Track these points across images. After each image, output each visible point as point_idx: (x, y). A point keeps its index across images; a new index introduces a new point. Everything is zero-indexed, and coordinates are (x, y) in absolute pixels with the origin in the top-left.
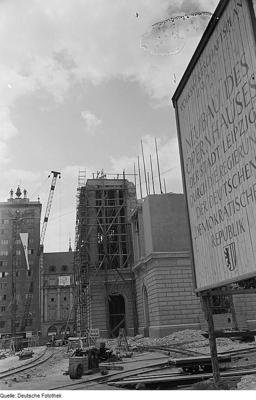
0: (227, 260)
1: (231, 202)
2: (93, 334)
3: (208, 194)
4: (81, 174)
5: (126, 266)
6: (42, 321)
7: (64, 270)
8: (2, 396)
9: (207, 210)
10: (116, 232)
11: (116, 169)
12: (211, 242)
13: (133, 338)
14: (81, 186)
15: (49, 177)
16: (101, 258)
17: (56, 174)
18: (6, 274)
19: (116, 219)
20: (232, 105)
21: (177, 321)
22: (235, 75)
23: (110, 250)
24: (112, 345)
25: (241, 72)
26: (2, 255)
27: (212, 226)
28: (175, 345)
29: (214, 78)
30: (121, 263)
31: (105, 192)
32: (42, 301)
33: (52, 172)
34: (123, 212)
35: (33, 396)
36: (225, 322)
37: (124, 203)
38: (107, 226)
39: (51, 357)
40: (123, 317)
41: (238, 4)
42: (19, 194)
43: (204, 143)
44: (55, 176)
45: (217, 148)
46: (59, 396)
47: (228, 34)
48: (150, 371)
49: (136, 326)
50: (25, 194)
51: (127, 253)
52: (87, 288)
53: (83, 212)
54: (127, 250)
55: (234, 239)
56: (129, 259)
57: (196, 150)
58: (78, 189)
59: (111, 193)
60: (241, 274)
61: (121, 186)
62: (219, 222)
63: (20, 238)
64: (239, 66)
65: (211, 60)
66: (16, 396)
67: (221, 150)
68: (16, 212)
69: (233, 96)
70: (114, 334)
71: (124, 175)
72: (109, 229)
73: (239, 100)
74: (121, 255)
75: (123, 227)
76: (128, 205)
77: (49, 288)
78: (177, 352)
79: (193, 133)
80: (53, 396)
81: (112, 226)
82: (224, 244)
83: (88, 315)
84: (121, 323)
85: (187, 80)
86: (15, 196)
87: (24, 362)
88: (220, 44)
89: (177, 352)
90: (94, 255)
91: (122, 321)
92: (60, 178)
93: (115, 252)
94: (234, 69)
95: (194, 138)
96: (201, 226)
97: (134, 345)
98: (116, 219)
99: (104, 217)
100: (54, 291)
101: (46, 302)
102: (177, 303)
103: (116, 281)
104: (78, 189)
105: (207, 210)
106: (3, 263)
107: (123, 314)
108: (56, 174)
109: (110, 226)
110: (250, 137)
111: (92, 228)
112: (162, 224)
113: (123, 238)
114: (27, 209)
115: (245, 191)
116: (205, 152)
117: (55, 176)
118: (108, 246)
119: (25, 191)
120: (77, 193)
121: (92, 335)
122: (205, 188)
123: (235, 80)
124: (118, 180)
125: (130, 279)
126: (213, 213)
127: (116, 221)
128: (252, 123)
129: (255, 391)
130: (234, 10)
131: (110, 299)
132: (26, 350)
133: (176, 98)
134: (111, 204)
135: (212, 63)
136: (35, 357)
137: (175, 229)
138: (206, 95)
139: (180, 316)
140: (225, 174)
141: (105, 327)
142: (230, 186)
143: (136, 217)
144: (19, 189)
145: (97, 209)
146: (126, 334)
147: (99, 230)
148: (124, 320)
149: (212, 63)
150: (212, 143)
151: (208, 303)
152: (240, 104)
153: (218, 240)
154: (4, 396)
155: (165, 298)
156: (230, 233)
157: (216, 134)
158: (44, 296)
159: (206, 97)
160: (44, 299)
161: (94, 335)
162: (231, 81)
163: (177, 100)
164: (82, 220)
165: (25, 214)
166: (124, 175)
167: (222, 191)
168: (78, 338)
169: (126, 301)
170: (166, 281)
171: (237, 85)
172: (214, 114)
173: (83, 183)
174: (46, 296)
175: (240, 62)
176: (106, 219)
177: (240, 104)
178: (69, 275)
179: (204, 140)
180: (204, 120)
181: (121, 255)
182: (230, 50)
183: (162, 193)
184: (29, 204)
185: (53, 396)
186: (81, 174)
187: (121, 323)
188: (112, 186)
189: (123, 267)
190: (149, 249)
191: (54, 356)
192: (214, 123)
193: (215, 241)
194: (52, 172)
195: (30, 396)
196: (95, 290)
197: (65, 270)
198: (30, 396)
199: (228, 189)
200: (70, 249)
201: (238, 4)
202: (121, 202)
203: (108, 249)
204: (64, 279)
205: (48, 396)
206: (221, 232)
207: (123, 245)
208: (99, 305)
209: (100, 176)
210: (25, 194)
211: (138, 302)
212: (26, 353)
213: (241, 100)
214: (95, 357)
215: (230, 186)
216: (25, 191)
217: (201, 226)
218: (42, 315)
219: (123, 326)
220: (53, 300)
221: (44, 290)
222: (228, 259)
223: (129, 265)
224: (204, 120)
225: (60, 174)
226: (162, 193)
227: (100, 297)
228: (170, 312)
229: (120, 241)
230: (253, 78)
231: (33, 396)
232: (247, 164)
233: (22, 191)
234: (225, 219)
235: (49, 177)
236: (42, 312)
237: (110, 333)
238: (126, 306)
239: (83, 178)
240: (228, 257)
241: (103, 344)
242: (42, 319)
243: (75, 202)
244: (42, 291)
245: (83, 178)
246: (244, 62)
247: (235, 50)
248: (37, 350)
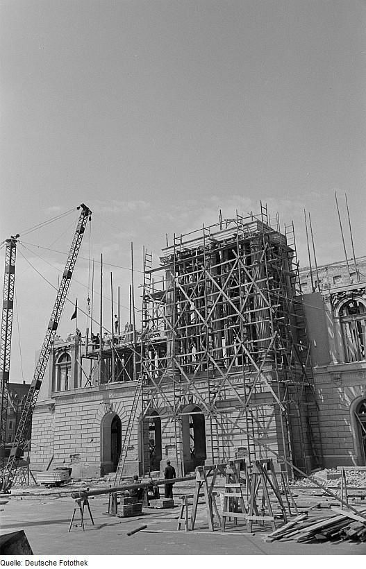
8: (3, 563)
35: (47, 563)
46: (84, 563)
66: (23, 563)
80: (75, 563)
185: (75, 563)
195: (43, 564)
198: (43, 564)
205: (68, 563)
231: (47, 563)
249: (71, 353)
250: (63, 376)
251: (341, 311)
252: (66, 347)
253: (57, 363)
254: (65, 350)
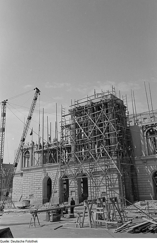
8: (1, 241)
33: (37, 88)
35: (20, 242)
46: (36, 242)
48: (147, 143)
66: (10, 242)
73: (76, 209)
80: (32, 241)
108: (38, 91)
129: (156, 239)
137: (113, 178)
166: (107, 188)
185: (32, 241)
195: (18, 242)
198: (18, 242)
205: (29, 241)
231: (20, 242)
249: (30, 151)
250: (26, 161)
251: (147, 135)
252: (28, 148)
253: (24, 155)
254: (27, 150)
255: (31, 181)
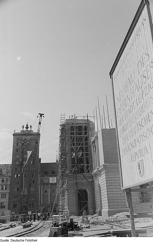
0: (139, 170)
1: (141, 135)
2: (65, 213)
3: (129, 130)
4: (62, 116)
5: (88, 172)
6: (39, 205)
7: (53, 173)
8: (1, 240)
9: (128, 140)
10: (83, 151)
11: (80, 114)
12: (130, 159)
13: (91, 216)
14: (62, 124)
15: (38, 117)
16: (73, 167)
17: (41, 115)
18: (19, 175)
19: (83, 143)
20: (141, 78)
21: (120, 206)
22: (143, 60)
23: (79, 161)
24: (78, 220)
25: (145, 59)
26: (17, 164)
27: (131, 149)
28: (117, 221)
29: (131, 62)
30: (85, 170)
31: (76, 127)
32: (40, 192)
33: (39, 114)
34: (87, 139)
35: (20, 241)
36: (148, 207)
37: (87, 134)
38: (77, 148)
39: (42, 227)
40: (86, 203)
41: (144, 19)
42: (27, 128)
43: (126, 99)
44: (41, 116)
45: (133, 103)
46: (36, 241)
47: (139, 36)
49: (94, 209)
50: (31, 128)
51: (89, 164)
52: (65, 185)
53: (63, 140)
54: (89, 162)
55: (143, 158)
56: (90, 167)
57: (122, 104)
58: (60, 125)
59: (80, 128)
60: (147, 179)
61: (86, 124)
62: (135, 147)
63: (27, 154)
64: (144, 56)
65: (130, 52)
66: (10, 241)
67: (135, 104)
68: (25, 138)
69: (141, 73)
70: (80, 214)
71: (87, 117)
72: (78, 149)
74: (85, 165)
75: (87, 148)
76: (90, 135)
77: (44, 184)
78: (117, 226)
79: (121, 94)
80: (32, 240)
81: (80, 148)
82: (138, 160)
83: (65, 201)
84: (85, 207)
85: (117, 63)
86: (25, 129)
87: (26, 229)
88: (135, 42)
89: (117, 226)
90: (69, 164)
91: (86, 206)
92: (44, 117)
93: (82, 163)
94: (142, 57)
95: (121, 97)
96: (125, 149)
97: (92, 221)
98: (83, 143)
99: (75, 142)
100: (47, 186)
101: (42, 194)
102: (119, 195)
103: (82, 181)
104: (60, 125)
105: (128, 140)
106: (17, 169)
107: (86, 201)
109: (79, 148)
110: (150, 97)
111: (68, 148)
112: (110, 147)
113: (87, 155)
114: (32, 137)
115: (148, 129)
116: (127, 105)
117: (41, 116)
118: (78, 159)
119: (31, 126)
120: (60, 127)
121: (65, 214)
122: (127, 126)
123: (143, 64)
124: (84, 120)
125: (91, 180)
126: (132, 141)
127: (82, 145)
128: (151, 88)
129: (152, 238)
130: (142, 23)
131: (78, 192)
132: (28, 222)
133: (111, 73)
134: (80, 134)
135: (130, 53)
136: (32, 226)
138: (127, 71)
139: (120, 204)
140: (138, 118)
141: (75, 209)
142: (140, 125)
143: (94, 142)
144: (27, 125)
145: (71, 137)
146: (88, 214)
147: (72, 149)
148: (87, 205)
149: (130, 53)
150: (130, 99)
151: (129, 196)
152: (145, 77)
153: (134, 158)
154: (2, 241)
155: (112, 192)
156: (141, 154)
157: (132, 95)
158: (41, 189)
159: (127, 72)
160: (41, 191)
161: (66, 214)
162: (140, 64)
163: (112, 75)
164: (62, 144)
165: (30, 140)
166: (87, 117)
167: (136, 128)
168: (58, 216)
169: (88, 193)
170: (112, 182)
171: (144, 66)
172: (132, 83)
173: (64, 122)
174: (42, 189)
175: (145, 53)
176: (77, 143)
177: (145, 77)
178: (56, 177)
179: (127, 98)
180: (126, 86)
181: (85, 165)
182: (140, 46)
183: (110, 128)
184: (33, 133)
185: (32, 240)
186: (62, 116)
187: (85, 207)
188: (80, 123)
189: (87, 172)
190: (102, 162)
191: (43, 226)
192: (131, 88)
193: (132, 158)
194: (39, 114)
195: (18, 241)
196: (69, 186)
197: (54, 174)
198: (18, 241)
199: (139, 127)
200: (57, 161)
201: (144, 19)
202: (86, 133)
203: (78, 161)
204: (53, 179)
205: (29, 240)
206: (136, 153)
207: (86, 159)
208: (72, 195)
209: (73, 117)
210: (31, 128)
211: (95, 194)
212: (28, 224)
213: (146, 75)
214: (65, 227)
215: (140, 125)
216: (31, 126)
217: (125, 149)
218: (39, 201)
219: (86, 209)
220: (46, 191)
221: (41, 186)
222: (140, 169)
223: (90, 171)
224: (126, 86)
225: (44, 114)
226: (110, 128)
227: (73, 190)
228: (115, 201)
229: (85, 157)
230: (152, 63)
231: (20, 241)
232: (149, 113)
233: (29, 126)
234: (138, 146)
235: (38, 117)
236: (39, 199)
237: (79, 213)
238: (88, 197)
239: (63, 119)
240: (139, 168)
241: (72, 220)
242: (39, 203)
243: (58, 134)
244: (40, 186)
245: (63, 119)
246: (147, 53)
247: (142, 46)
248: (35, 223)
255: (116, 192)
